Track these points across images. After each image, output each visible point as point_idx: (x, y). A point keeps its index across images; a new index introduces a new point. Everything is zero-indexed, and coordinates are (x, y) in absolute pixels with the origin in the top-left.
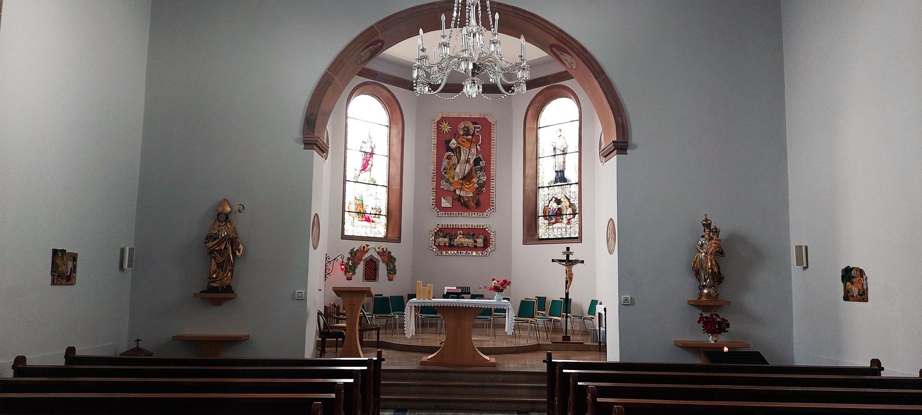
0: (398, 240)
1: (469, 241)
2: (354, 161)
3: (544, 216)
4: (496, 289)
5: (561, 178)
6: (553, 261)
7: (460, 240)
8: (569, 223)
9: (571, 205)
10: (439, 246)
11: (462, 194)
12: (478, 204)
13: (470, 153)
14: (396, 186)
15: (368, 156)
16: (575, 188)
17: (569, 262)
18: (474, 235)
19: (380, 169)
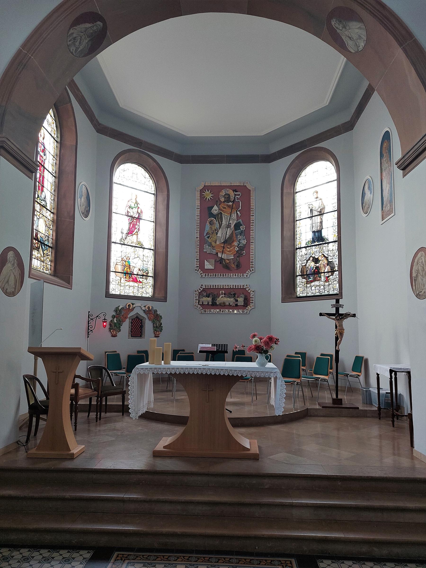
0: (165, 299)
1: (231, 301)
2: (119, 225)
3: (302, 275)
4: (258, 349)
5: (318, 238)
6: (321, 314)
7: (221, 299)
8: (327, 280)
9: (329, 263)
10: (202, 305)
11: (224, 256)
12: (238, 266)
13: (231, 219)
14: (162, 250)
15: (135, 221)
16: (333, 247)
17: (339, 316)
18: (234, 294)
19: (147, 233)
